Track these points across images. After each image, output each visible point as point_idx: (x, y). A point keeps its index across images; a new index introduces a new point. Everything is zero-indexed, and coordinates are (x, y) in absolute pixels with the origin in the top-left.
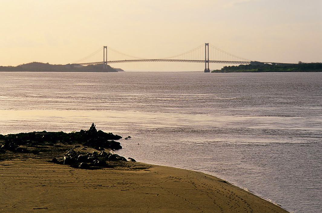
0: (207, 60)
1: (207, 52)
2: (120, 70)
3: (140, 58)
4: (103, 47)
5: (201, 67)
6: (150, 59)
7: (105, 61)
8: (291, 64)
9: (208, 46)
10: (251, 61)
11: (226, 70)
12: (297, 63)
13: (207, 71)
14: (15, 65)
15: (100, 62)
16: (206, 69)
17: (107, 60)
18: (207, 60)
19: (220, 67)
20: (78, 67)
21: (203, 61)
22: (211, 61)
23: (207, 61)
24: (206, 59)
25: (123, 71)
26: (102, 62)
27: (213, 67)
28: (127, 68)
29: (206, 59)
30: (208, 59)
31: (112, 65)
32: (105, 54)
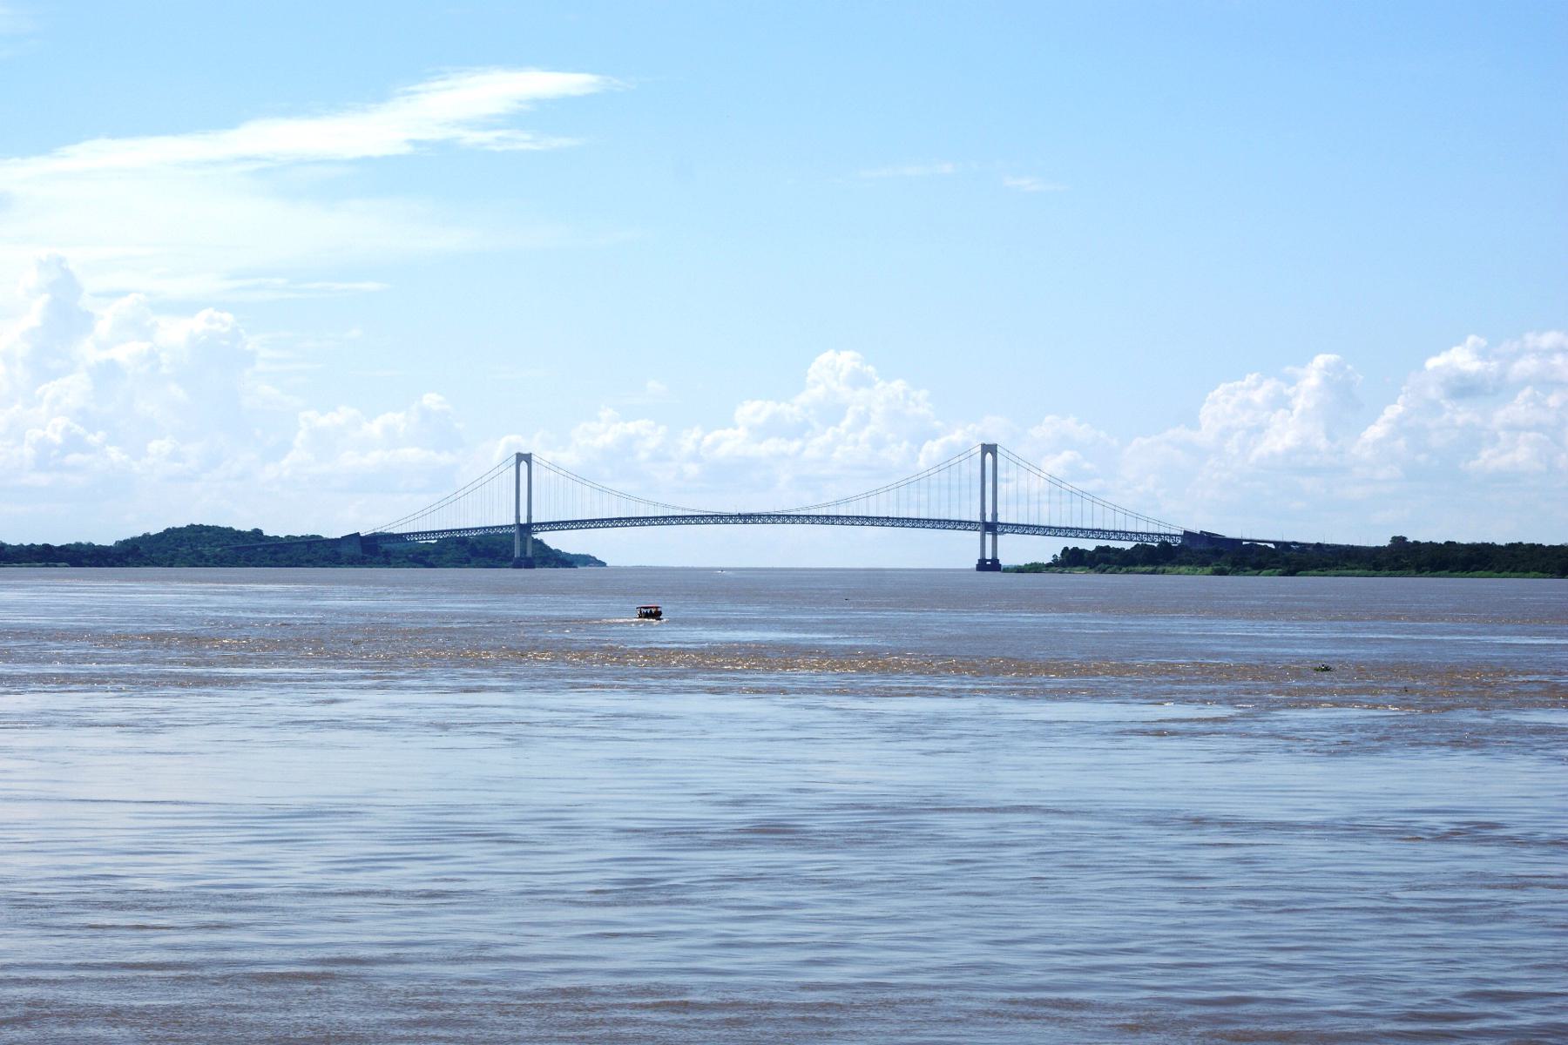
0: (989, 519)
1: (989, 480)
2: (587, 560)
3: (683, 509)
4: (514, 459)
5: (963, 551)
6: (734, 512)
7: (523, 521)
8: (1340, 546)
9: (994, 453)
10: (1185, 532)
11: (1072, 559)
12: (1385, 542)
13: (989, 565)
14: (106, 537)
15: (501, 527)
16: (995, 535)
17: (529, 517)
18: (989, 519)
19: (1046, 550)
20: (399, 546)
21: (970, 523)
22: (1007, 525)
23: (991, 528)
24: (983, 514)
25: (603, 564)
26: (510, 527)
27: (1012, 550)
28: (613, 548)
29: (983, 514)
30: (995, 515)
31: (554, 540)
32: (523, 489)
